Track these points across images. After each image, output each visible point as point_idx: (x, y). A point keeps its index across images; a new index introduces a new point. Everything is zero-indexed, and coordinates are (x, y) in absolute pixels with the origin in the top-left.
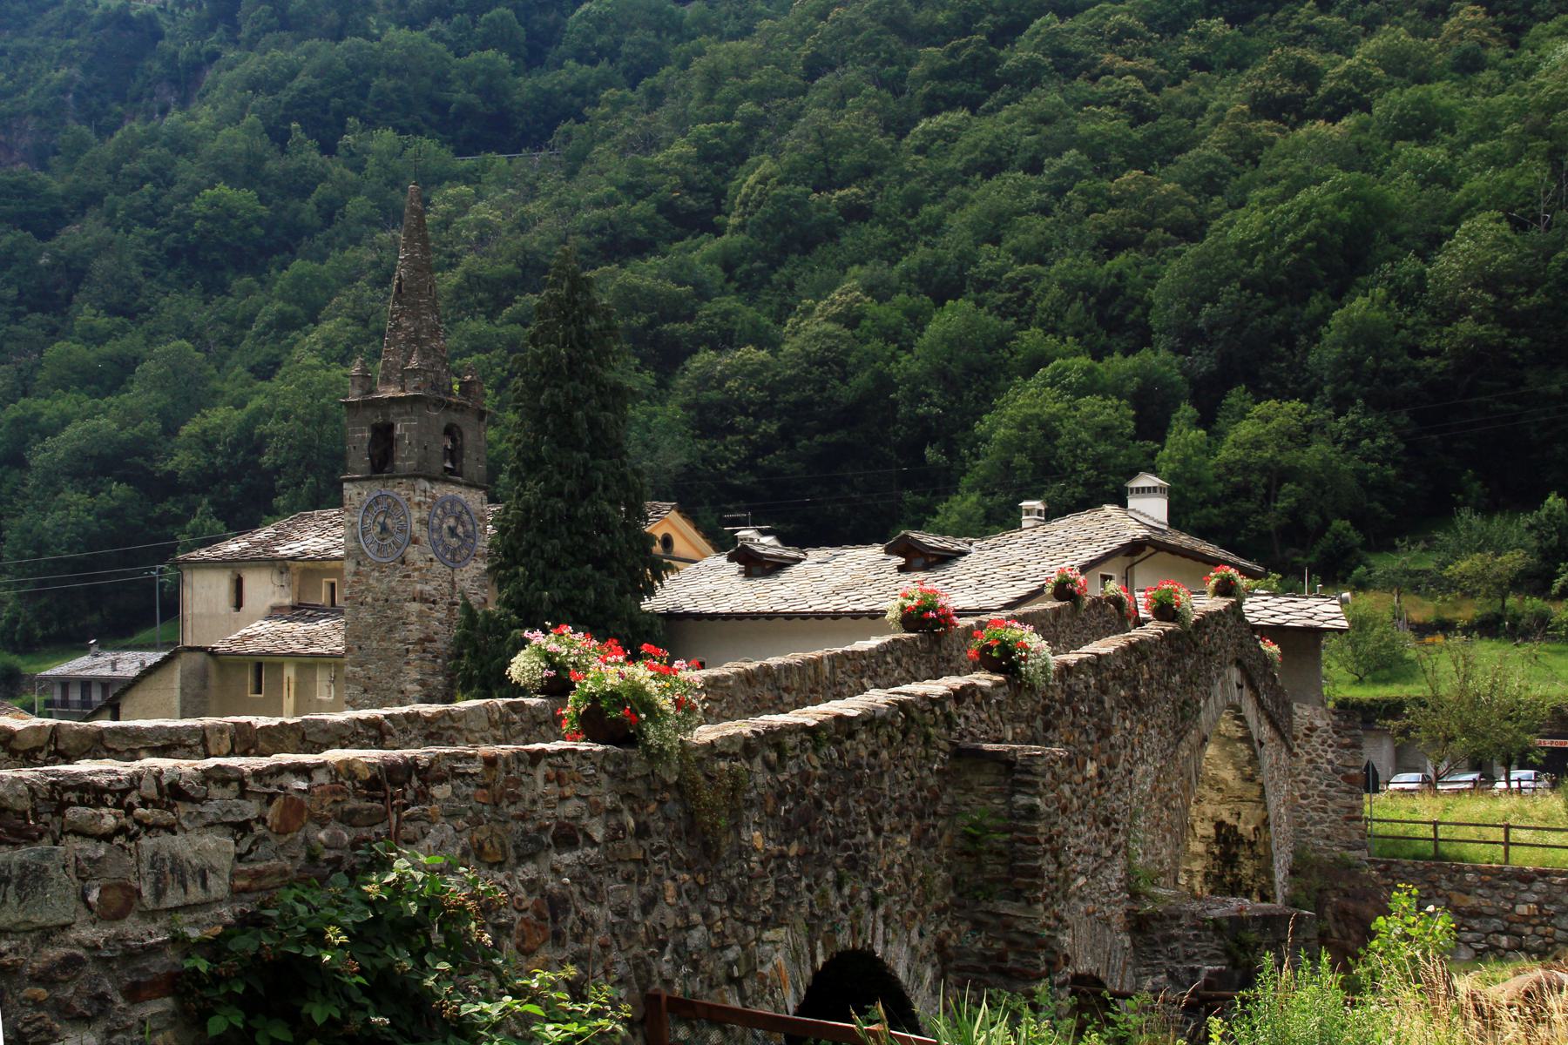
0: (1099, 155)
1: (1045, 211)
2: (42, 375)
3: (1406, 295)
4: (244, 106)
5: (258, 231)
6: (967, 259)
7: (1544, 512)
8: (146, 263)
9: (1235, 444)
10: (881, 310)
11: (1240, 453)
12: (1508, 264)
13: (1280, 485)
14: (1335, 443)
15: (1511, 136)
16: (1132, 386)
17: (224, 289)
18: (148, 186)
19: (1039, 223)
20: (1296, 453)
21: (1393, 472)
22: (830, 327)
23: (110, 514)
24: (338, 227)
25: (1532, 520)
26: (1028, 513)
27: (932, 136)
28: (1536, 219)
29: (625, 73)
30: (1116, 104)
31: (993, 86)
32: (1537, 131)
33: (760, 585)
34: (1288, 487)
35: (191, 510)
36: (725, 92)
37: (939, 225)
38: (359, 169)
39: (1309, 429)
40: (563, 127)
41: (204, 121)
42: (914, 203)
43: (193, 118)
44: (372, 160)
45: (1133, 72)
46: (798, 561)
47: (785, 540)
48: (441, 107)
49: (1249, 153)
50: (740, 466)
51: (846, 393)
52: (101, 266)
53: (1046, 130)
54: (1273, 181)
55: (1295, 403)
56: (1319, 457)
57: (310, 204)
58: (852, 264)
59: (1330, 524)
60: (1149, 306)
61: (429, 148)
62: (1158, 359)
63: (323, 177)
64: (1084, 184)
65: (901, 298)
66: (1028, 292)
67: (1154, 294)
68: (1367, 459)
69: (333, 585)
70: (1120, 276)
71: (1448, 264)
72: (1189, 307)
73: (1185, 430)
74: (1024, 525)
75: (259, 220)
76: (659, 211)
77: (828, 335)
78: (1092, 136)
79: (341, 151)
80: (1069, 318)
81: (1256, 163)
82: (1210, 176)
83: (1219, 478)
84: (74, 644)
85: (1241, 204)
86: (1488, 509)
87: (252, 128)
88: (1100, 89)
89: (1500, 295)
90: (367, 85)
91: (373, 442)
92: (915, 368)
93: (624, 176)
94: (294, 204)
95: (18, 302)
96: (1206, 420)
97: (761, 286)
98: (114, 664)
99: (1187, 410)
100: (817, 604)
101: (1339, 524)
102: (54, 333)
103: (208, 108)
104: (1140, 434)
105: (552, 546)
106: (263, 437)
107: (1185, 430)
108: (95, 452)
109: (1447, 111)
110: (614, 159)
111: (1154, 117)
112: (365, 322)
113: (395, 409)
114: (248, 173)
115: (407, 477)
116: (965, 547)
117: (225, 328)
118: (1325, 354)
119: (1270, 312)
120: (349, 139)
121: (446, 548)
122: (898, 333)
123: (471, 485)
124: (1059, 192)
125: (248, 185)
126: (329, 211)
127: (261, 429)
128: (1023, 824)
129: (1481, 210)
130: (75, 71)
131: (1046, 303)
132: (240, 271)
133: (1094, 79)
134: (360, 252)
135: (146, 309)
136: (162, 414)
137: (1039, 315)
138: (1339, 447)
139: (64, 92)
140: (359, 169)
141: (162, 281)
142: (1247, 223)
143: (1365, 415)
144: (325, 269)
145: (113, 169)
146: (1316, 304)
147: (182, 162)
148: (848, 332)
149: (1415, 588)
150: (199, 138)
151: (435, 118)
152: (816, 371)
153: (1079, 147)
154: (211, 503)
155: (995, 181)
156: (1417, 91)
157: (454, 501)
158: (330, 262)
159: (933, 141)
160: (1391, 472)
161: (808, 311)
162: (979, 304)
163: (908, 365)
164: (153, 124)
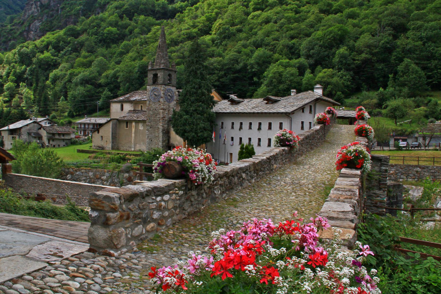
0: (289, 20)
1: (278, 31)
2: (75, 65)
3: (352, 49)
4: (114, 12)
5: (117, 36)
6: (263, 40)
7: (379, 92)
8: (95, 42)
10: (246, 50)
11: (320, 79)
12: (372, 43)
13: (327, 86)
15: (371, 19)
16: (297, 65)
17: (110, 47)
18: (96, 28)
19: (277, 33)
20: (331, 79)
22: (235, 53)
23: (88, 91)
24: (132, 34)
26: (293, 92)
27: (254, 16)
28: (376, 34)
29: (190, 4)
30: (292, 10)
31: (266, 6)
32: (376, 18)
33: (269, 106)
34: (329, 86)
35: (104, 90)
36: (211, 7)
37: (256, 33)
38: (137, 23)
40: (178, 14)
41: (107, 15)
42: (251, 29)
43: (104, 14)
44: (139, 22)
45: (295, 4)
46: (243, 101)
47: (239, 97)
48: (153, 11)
49: (319, 20)
50: (216, 81)
52: (87, 43)
53: (278, 15)
54: (324, 26)
57: (127, 30)
58: (239, 41)
60: (300, 50)
61: (151, 19)
62: (302, 60)
63: (129, 25)
64: (286, 26)
65: (249, 48)
66: (275, 47)
67: (301, 48)
69: (142, 106)
70: (294, 44)
71: (360, 43)
72: (308, 51)
75: (117, 34)
76: (199, 30)
77: (235, 55)
78: (287, 16)
79: (133, 20)
80: (284, 52)
81: (321, 22)
82: (311, 25)
84: (81, 116)
85: (318, 30)
86: (368, 90)
87: (116, 16)
88: (288, 7)
89: (370, 49)
90: (139, 7)
91: (153, 78)
92: (252, 62)
93: (191, 24)
94: (124, 30)
95: (71, 51)
96: (313, 72)
97: (219, 45)
98: (90, 120)
99: (309, 70)
100: (249, 111)
102: (77, 56)
103: (107, 12)
104: (300, 75)
105: (193, 98)
106: (118, 76)
108: (85, 79)
109: (358, 13)
110: (189, 20)
111: (300, 13)
112: (139, 53)
113: (158, 71)
114: (115, 24)
115: (161, 85)
116: (279, 99)
117: (110, 55)
118: (336, 59)
119: (325, 51)
120: (135, 18)
121: (168, 98)
122: (249, 55)
123: (173, 86)
124: (281, 27)
125: (115, 27)
126: (131, 32)
127: (118, 74)
128: (384, 173)
129: (366, 32)
130: (82, 7)
131: (279, 49)
132: (113, 44)
133: (287, 5)
134: (137, 39)
135: (95, 51)
136: (98, 72)
137: (278, 51)
139: (80, 11)
140: (137, 23)
141: (98, 46)
142: (320, 33)
143: (344, 72)
144: (130, 43)
145: (89, 25)
146: (333, 50)
147: (102, 23)
148: (238, 54)
150: (106, 18)
151: (152, 13)
152: (232, 62)
153: (285, 19)
154: (108, 89)
155: (267, 25)
156: (351, 9)
157: (170, 89)
158: (131, 41)
159: (254, 17)
160: (349, 83)
161: (230, 50)
162: (266, 49)
163: (252, 61)
164: (97, 16)
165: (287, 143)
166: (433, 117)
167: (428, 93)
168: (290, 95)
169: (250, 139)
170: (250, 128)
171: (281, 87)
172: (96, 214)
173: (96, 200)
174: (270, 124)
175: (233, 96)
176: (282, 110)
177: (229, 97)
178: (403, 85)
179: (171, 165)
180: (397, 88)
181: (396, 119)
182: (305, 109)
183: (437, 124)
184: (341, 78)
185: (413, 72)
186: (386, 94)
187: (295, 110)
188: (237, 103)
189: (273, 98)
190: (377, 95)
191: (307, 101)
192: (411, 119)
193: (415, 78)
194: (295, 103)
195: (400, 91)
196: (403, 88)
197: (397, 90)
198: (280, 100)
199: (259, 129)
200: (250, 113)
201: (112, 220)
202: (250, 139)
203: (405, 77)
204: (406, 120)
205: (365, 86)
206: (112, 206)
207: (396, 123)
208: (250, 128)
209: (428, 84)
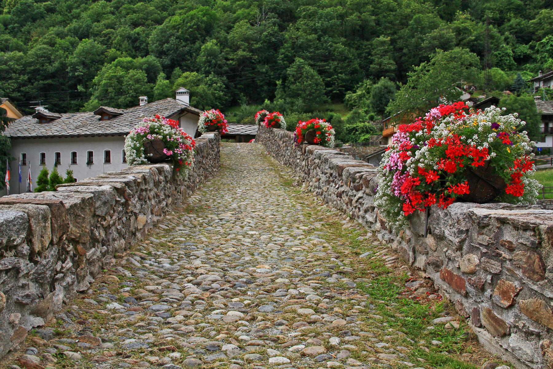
25: (261, 107)
26: (142, 100)
33: (103, 123)
39: (199, 80)
46: (60, 118)
51: (51, 68)
100: (71, 132)
104: (149, 82)
116: (121, 112)
138: (207, 86)
163: (73, 59)
165: (165, 151)
167: (327, 106)
174: (108, 154)
175: (41, 109)
178: (296, 95)
180: (288, 100)
185: (307, 78)
193: (310, 85)
195: (292, 104)
196: (295, 100)
197: (288, 103)
198: (122, 114)
199: (90, 162)
200: (72, 136)
203: (298, 84)
209: (327, 94)
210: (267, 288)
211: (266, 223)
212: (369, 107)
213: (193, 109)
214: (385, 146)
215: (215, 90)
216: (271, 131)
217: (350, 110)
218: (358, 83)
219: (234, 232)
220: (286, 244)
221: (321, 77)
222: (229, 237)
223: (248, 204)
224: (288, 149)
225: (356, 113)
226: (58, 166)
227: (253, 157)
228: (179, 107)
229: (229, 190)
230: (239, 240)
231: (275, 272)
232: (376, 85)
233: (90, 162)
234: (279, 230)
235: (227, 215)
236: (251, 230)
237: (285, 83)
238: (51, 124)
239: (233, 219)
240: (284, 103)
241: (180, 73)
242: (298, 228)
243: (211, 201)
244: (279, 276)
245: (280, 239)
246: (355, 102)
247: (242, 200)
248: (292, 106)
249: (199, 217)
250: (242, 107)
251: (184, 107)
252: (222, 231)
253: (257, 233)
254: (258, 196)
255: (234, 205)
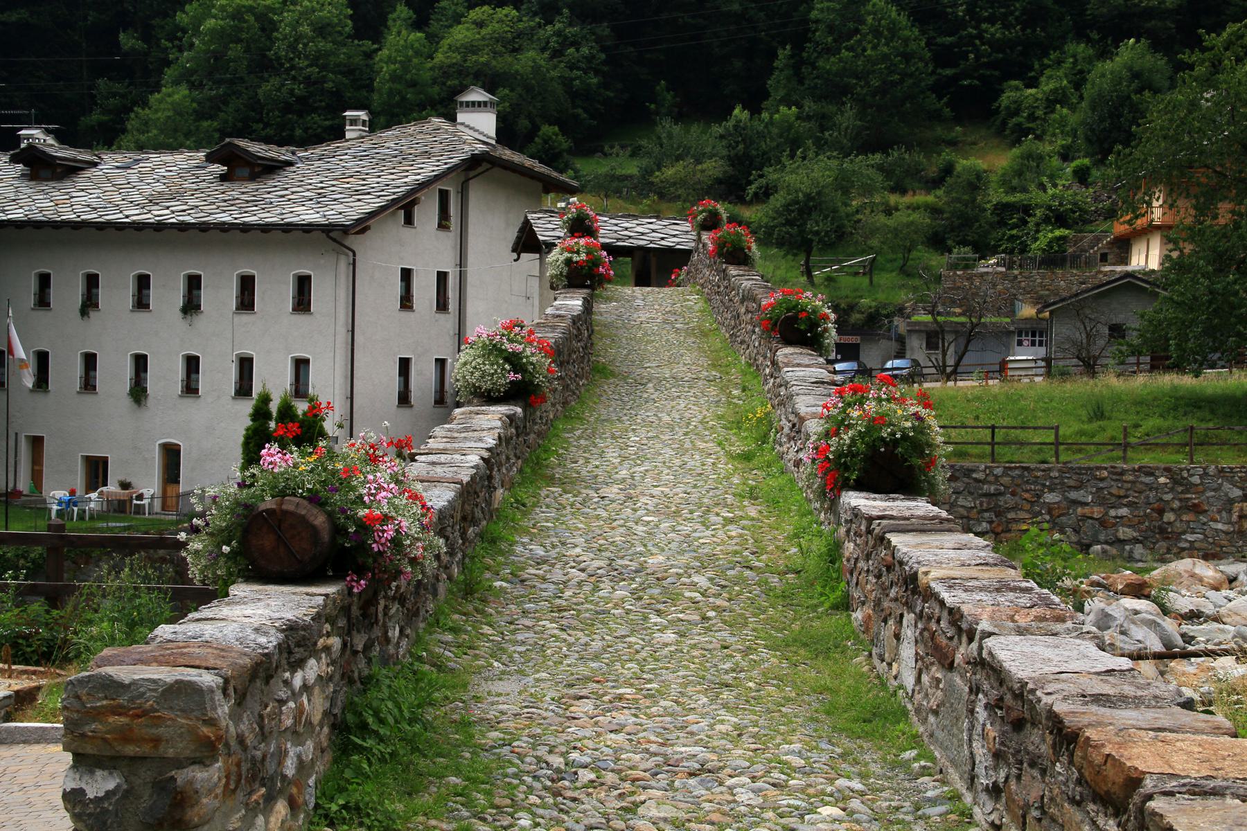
7: (730, 124)
9: (450, 46)
11: (456, 58)
14: (543, 50)
21: (595, 81)
25: (721, 131)
26: (354, 122)
33: (236, 191)
39: (520, 35)
46: (95, 165)
47: (64, 138)
55: (506, 10)
56: (531, 63)
59: (539, 129)
68: (572, 67)
73: (404, 32)
74: (348, 135)
83: (434, 81)
86: (680, 117)
100: (134, 214)
101: (548, 130)
104: (358, 34)
107: (404, 32)
116: (288, 157)
138: (546, 55)
143: (571, 25)
149: (618, 192)
166: (964, 243)
167: (939, 131)
168: (339, 134)
169: (301, 365)
170: (141, 303)
171: (269, 87)
172: (111, 785)
173: (117, 711)
174: (247, 284)
175: (35, 135)
176: (309, 215)
177: (19, 139)
178: (835, 91)
179: (286, 513)
180: (809, 106)
181: (809, 254)
182: (417, 211)
183: (982, 275)
184: (557, 53)
185: (877, 33)
186: (761, 136)
187: (372, 215)
188: (67, 171)
189: (257, 148)
190: (722, 137)
191: (428, 169)
192: (870, 250)
193: (885, 57)
194: (372, 180)
195: (823, 121)
196: (832, 108)
197: (809, 118)
198: (290, 164)
199: (191, 306)
200: (139, 227)
201: (205, 801)
202: (301, 365)
203: (845, 53)
204: (853, 255)
205: (669, 96)
206: (205, 730)
207: (808, 273)
208: (141, 303)
209: (939, 88)
210: (659, 576)
211: (672, 505)
212: (1074, 134)
213: (507, 154)
214: (1119, 269)
215: (572, 67)
216: (724, 271)
217: (1013, 145)
218: (1047, 55)
219: (622, 516)
220: (694, 535)
221: (923, 32)
222: (615, 524)
223: (647, 471)
224: (754, 332)
225: (1029, 156)
226: (92, 314)
227: (672, 336)
228: (467, 148)
229: (613, 437)
230: (629, 528)
231: (669, 563)
232: (1108, 65)
233: (191, 306)
234: (689, 516)
235: (612, 491)
236: (647, 515)
237: (803, 49)
238: (68, 183)
239: (621, 496)
240: (798, 118)
241: (460, 9)
242: (718, 515)
243: (581, 462)
244: (672, 566)
245: (686, 528)
246: (1032, 117)
247: (639, 462)
248: (823, 129)
249: (566, 492)
250: (659, 129)
251: (481, 147)
252: (604, 514)
253: (656, 519)
254: (668, 452)
255: (624, 473)
